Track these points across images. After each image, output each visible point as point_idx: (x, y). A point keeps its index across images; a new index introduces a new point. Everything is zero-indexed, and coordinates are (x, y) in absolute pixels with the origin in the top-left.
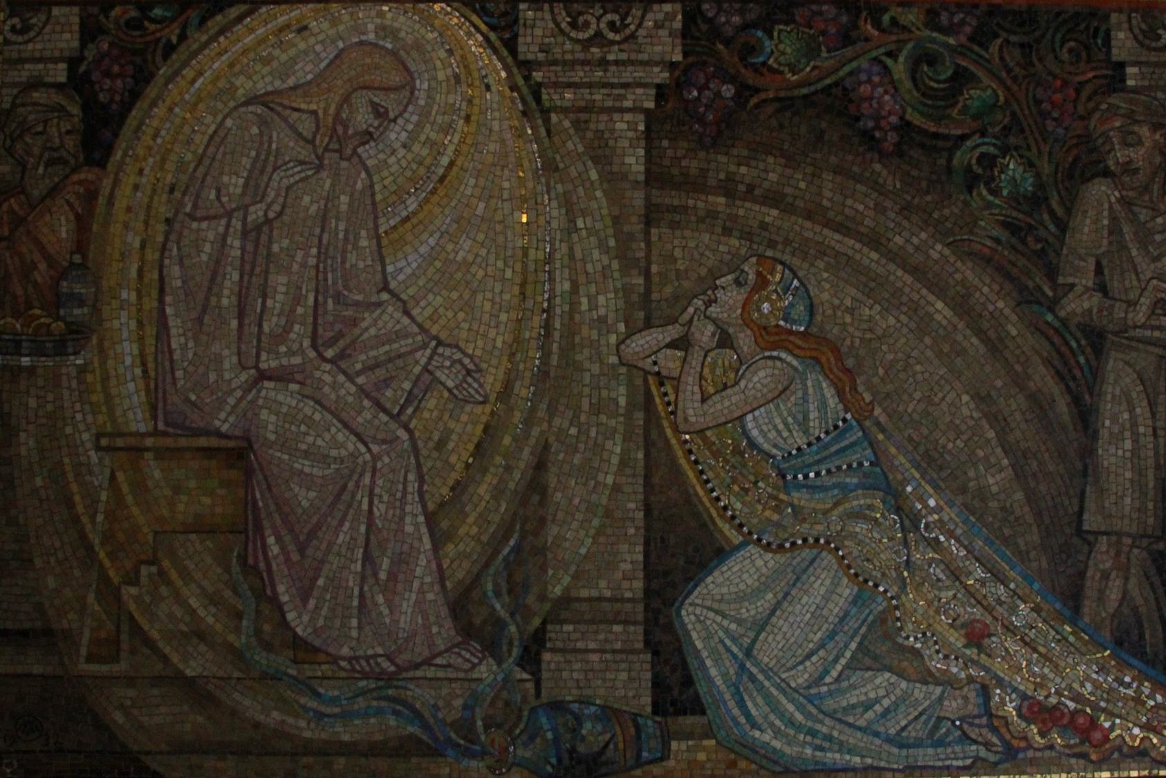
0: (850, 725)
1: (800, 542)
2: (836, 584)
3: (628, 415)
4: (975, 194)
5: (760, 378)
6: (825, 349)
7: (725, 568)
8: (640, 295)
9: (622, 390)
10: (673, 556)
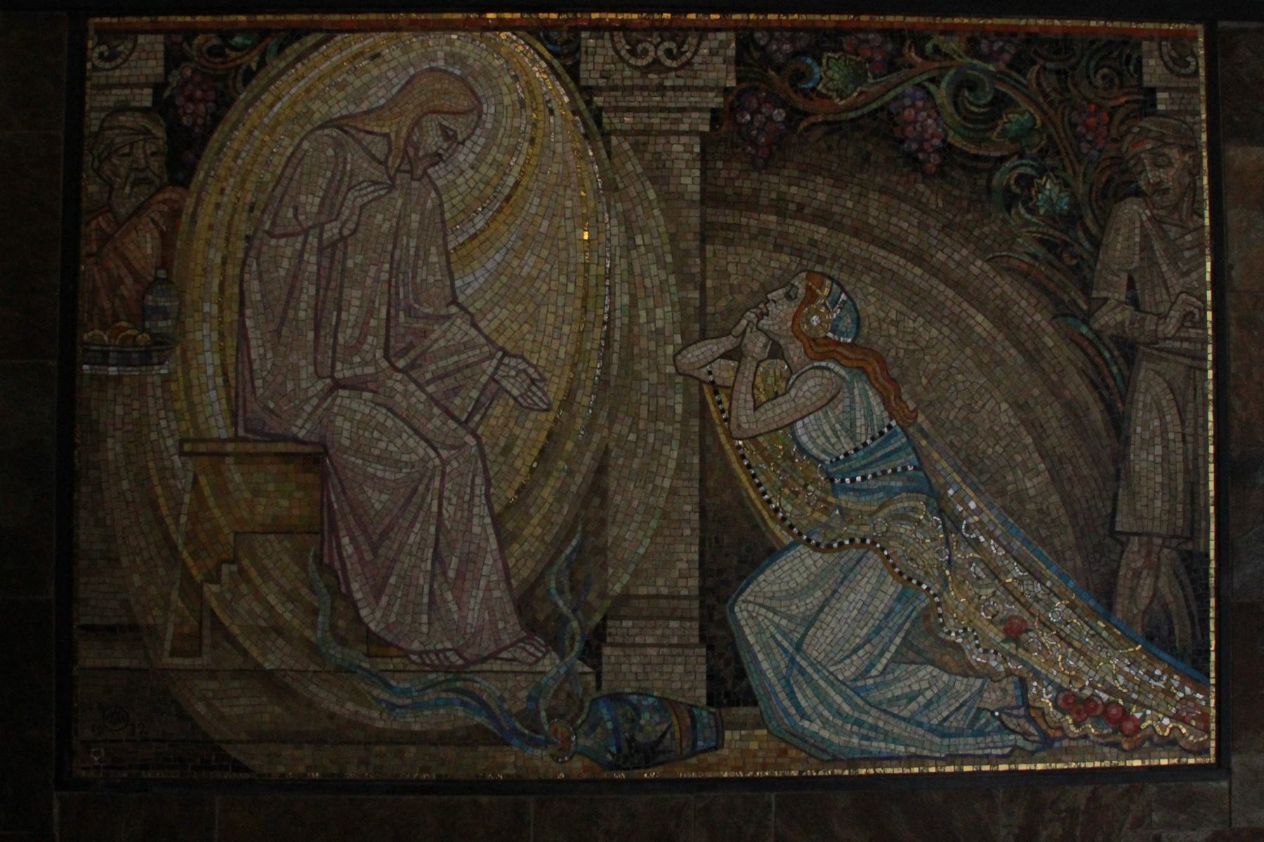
0: (895, 716)
2: (881, 582)
3: (684, 422)
4: (1013, 212)
5: (810, 387)
7: (776, 567)
8: (695, 308)
9: (679, 398)
10: (727, 555)
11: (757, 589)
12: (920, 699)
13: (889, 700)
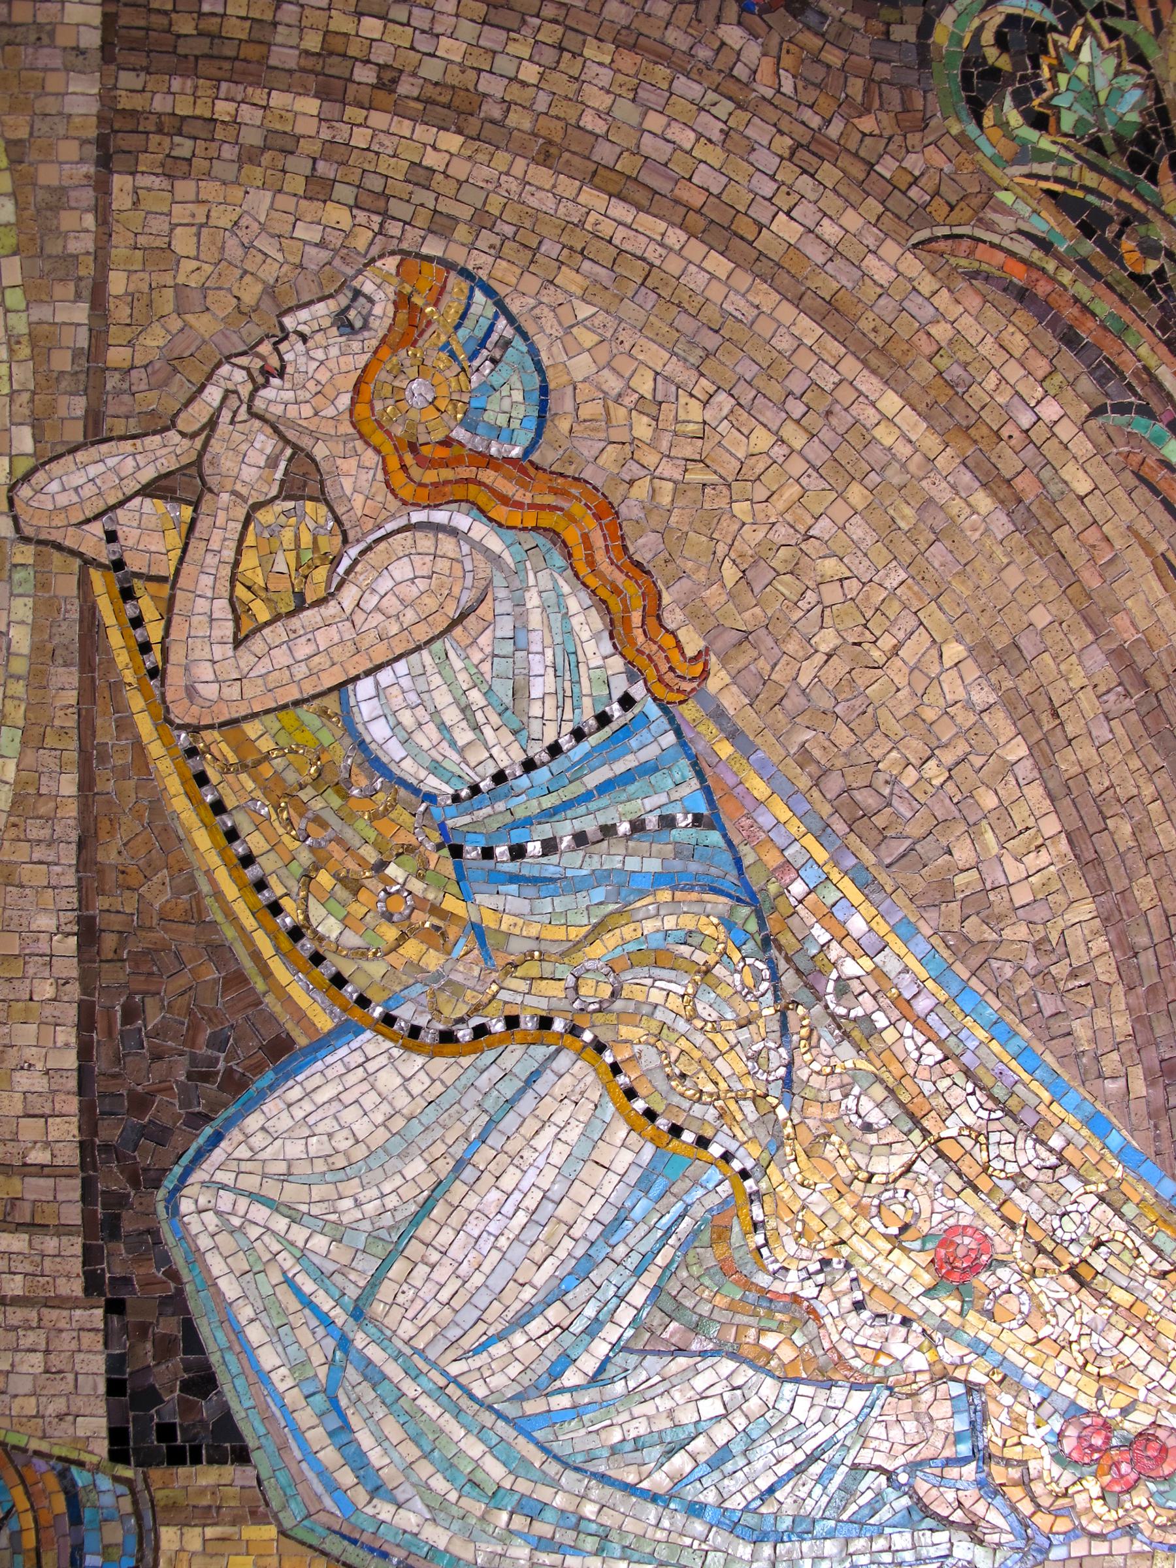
0: (630, 1489)
1: (498, 1027)
2: (594, 1138)
3: (37, 679)
4: (988, 119)
5: (397, 582)
6: (577, 509)
7: (296, 1093)
8: (77, 354)
9: (22, 609)
10: (157, 1057)
11: (243, 1152)
12: (699, 1444)
13: (614, 1450)
